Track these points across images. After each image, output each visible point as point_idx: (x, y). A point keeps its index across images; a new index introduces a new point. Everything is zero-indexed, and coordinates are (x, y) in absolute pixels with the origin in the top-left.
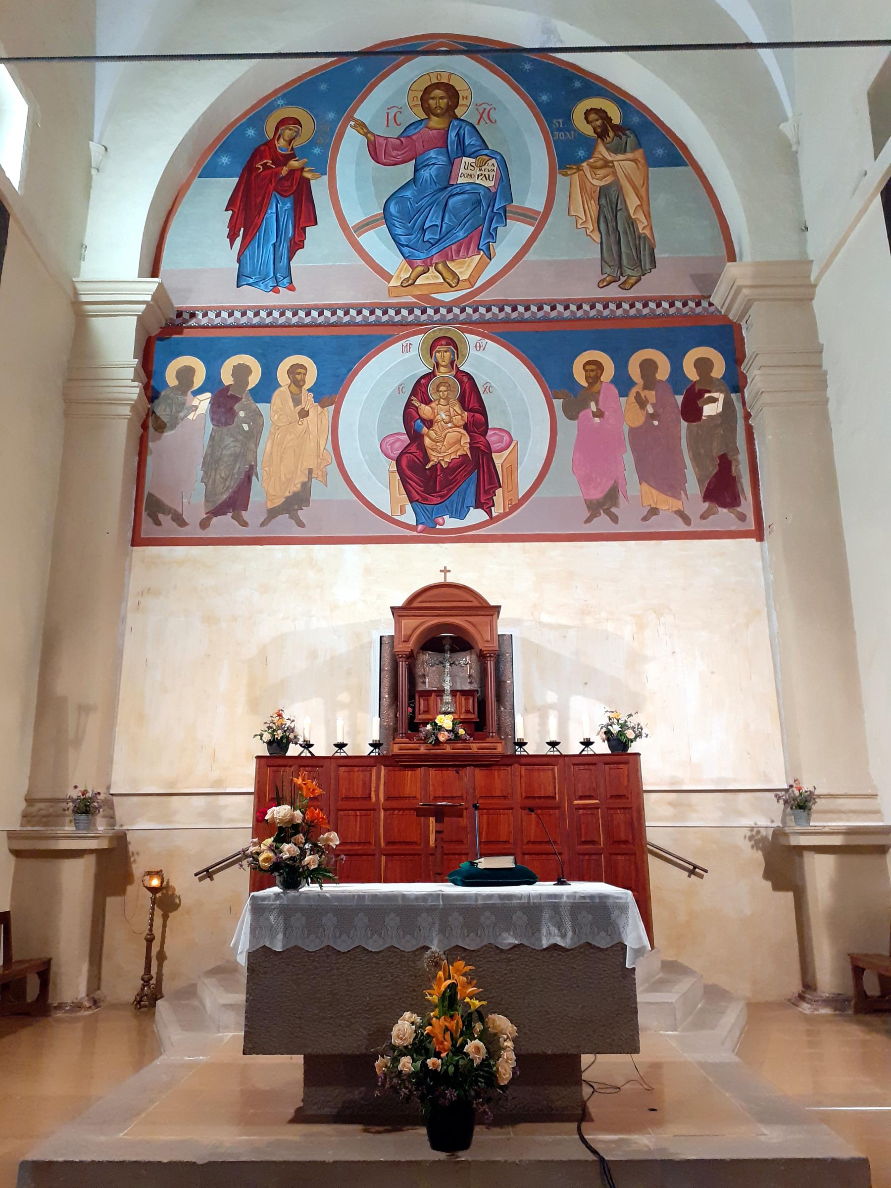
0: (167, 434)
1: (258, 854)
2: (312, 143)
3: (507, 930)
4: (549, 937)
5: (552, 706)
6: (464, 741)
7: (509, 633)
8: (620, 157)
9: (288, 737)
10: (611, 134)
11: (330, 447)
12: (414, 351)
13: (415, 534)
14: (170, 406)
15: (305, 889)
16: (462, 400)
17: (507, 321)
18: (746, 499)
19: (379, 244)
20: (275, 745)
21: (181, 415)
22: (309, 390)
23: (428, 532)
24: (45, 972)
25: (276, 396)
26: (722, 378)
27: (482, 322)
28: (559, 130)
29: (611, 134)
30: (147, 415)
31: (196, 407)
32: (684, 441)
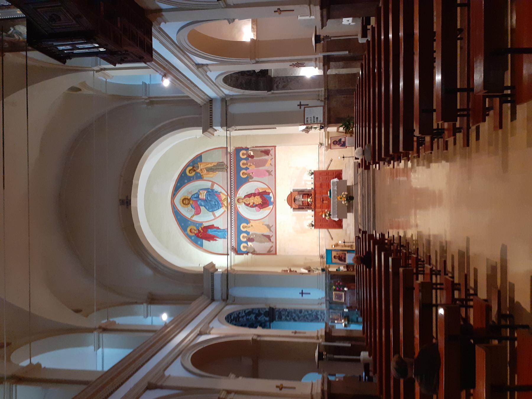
0: (256, 250)
2: (196, 226)
4: (336, 188)
16: (249, 197)
19: (218, 213)
23: (274, 203)
25: (248, 231)
27: (234, 194)
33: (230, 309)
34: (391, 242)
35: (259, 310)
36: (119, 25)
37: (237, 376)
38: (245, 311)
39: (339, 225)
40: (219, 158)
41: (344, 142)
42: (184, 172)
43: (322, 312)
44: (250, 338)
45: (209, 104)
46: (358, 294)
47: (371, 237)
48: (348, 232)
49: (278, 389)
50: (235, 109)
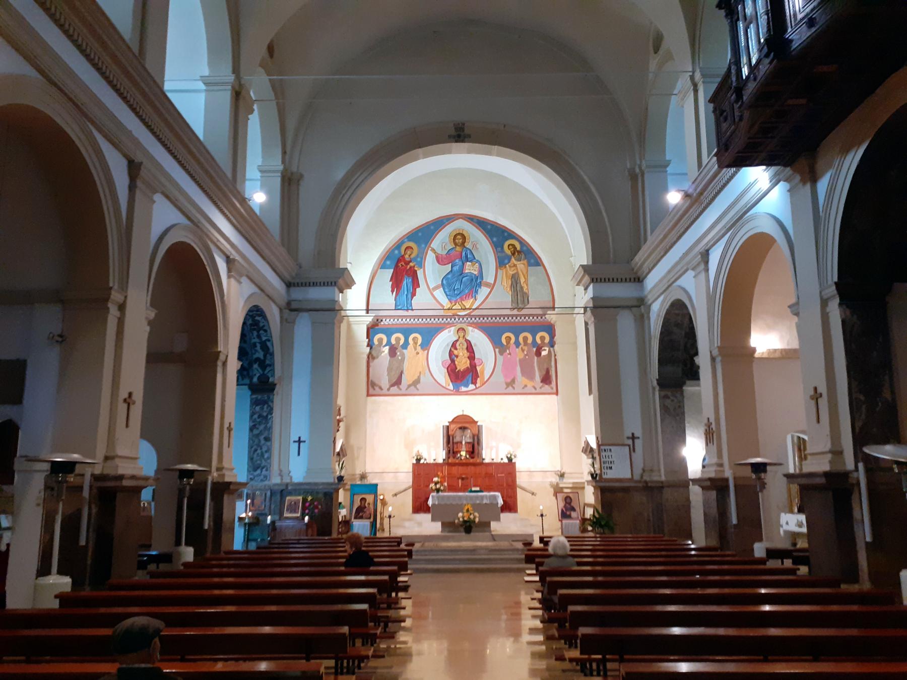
0: (376, 361)
2: (417, 256)
4: (485, 501)
17: (482, 323)
19: (440, 294)
23: (457, 392)
27: (473, 323)
33: (273, 314)
34: (394, 604)
35: (272, 365)
36: (790, 102)
37: (150, 323)
38: (269, 340)
39: (420, 506)
40: (537, 296)
41: (569, 517)
42: (511, 235)
43: (266, 477)
44: (220, 348)
45: (632, 277)
46: (298, 542)
47: (403, 567)
48: (407, 524)
49: (126, 396)
50: (626, 323)
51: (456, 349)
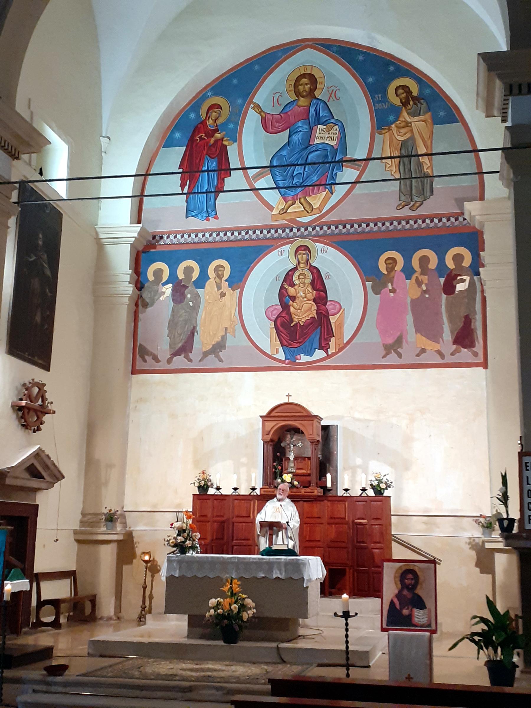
0: (149, 309)
1: (170, 540)
2: (228, 121)
3: (260, 571)
5: (359, 467)
6: (297, 488)
7: (336, 424)
8: (416, 119)
9: (207, 485)
10: (411, 103)
11: (237, 314)
12: (285, 255)
13: (284, 365)
14: (150, 292)
15: (188, 555)
18: (478, 343)
20: (201, 489)
21: (156, 297)
22: (226, 281)
23: (292, 365)
24: (93, 600)
26: (470, 266)
27: (325, 235)
28: (379, 102)
29: (411, 103)
30: (138, 298)
31: (164, 293)
32: (443, 307)
42: (402, 69)
51: (293, 285)
